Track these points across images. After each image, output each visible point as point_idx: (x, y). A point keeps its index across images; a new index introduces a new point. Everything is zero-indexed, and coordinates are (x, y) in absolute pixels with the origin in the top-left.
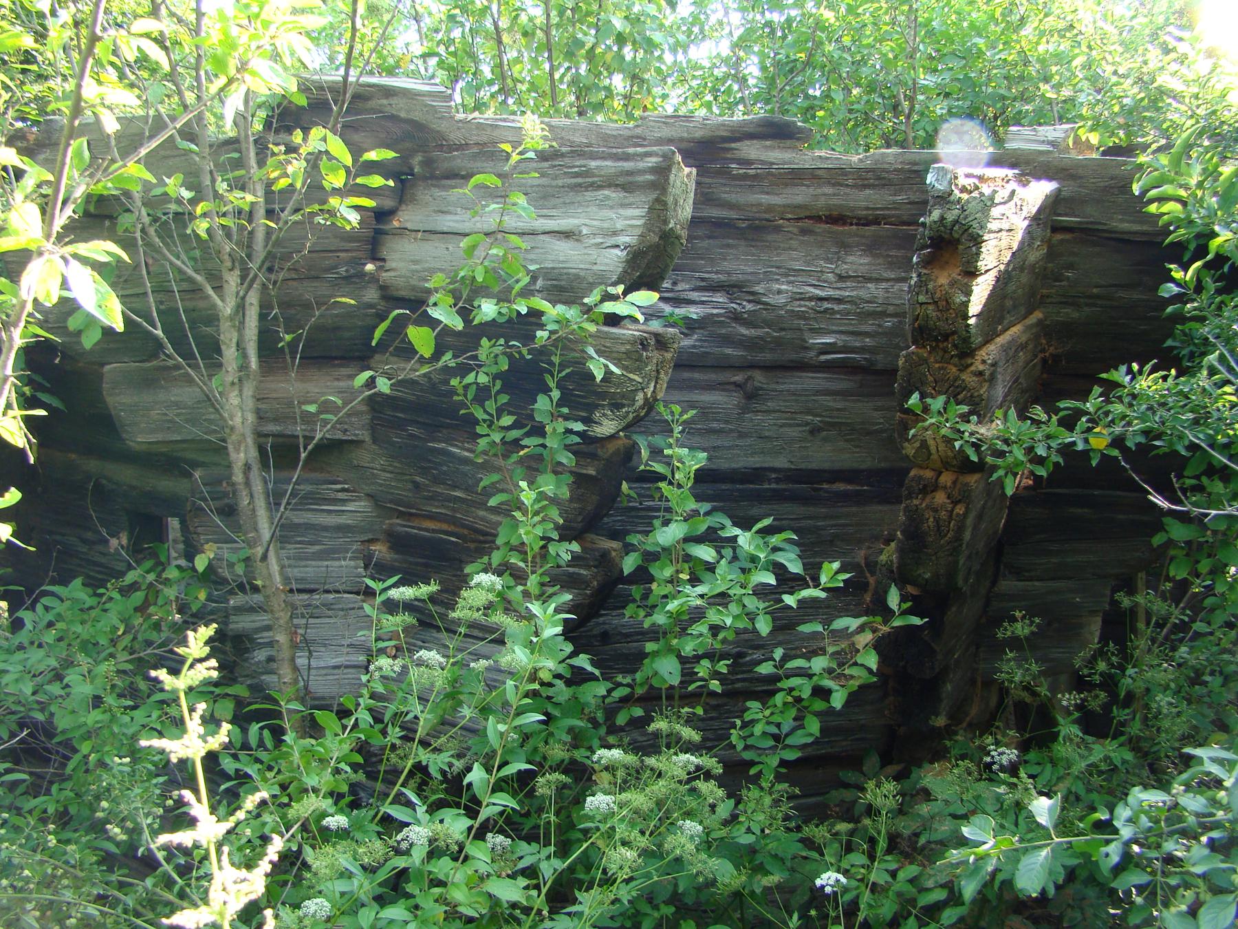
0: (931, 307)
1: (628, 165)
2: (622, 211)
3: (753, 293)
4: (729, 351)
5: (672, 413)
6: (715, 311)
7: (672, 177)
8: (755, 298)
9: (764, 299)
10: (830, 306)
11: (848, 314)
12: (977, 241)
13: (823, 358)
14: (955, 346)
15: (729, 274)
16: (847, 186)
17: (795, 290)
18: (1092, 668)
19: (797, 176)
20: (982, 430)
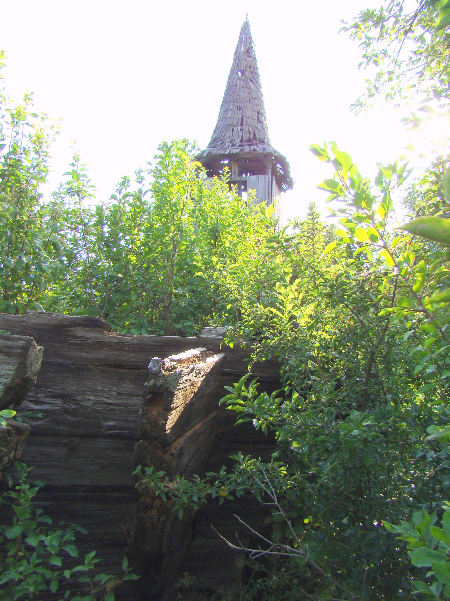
0: (148, 425)
1: (10, 343)
2: (4, 366)
3: (76, 400)
4: (62, 428)
5: (22, 467)
6: (56, 408)
7: (30, 352)
8: (76, 402)
9: (81, 403)
10: (113, 407)
11: (122, 411)
12: (172, 395)
13: (109, 432)
14: (160, 443)
15: (64, 390)
16: (125, 351)
17: (97, 399)
18: (285, 523)
19: (101, 345)
20: (171, 485)
